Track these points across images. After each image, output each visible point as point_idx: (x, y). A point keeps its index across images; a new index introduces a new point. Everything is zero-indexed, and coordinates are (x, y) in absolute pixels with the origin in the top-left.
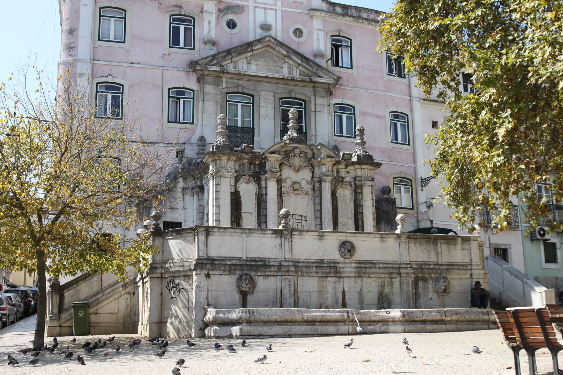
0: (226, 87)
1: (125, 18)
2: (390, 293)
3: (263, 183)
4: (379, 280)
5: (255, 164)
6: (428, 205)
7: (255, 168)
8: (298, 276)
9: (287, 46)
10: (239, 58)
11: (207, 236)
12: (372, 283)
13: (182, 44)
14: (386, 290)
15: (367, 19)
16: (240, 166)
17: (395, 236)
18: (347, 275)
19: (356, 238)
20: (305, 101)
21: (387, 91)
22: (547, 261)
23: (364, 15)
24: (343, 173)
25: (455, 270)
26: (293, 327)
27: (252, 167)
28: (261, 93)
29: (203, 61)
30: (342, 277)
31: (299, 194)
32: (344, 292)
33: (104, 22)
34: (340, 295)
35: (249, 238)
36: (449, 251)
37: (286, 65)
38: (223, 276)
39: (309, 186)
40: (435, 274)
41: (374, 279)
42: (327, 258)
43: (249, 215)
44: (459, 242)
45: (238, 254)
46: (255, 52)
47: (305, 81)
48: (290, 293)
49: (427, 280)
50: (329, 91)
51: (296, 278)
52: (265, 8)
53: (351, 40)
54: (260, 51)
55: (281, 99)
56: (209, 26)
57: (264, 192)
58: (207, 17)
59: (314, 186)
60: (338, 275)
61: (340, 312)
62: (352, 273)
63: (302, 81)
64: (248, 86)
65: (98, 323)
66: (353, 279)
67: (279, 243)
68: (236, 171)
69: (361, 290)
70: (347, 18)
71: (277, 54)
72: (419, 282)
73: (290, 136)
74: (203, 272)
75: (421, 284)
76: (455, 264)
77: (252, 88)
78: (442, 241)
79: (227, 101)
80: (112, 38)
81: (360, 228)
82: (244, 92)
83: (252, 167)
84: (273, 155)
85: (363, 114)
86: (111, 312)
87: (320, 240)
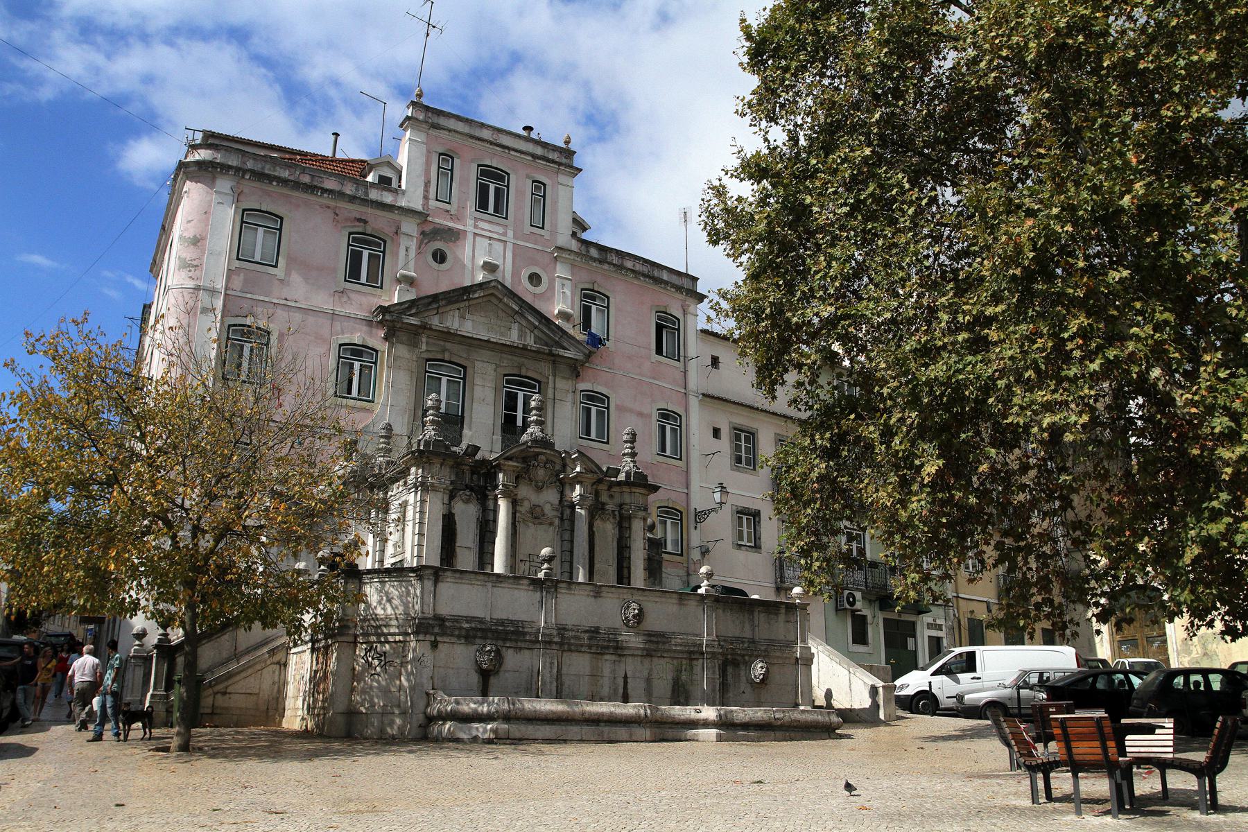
0: (427, 351)
1: (280, 230)
3: (491, 504)
4: (675, 662)
5: (478, 474)
6: (703, 550)
7: (479, 480)
8: (563, 651)
9: (520, 299)
10: (448, 308)
11: (436, 582)
13: (363, 279)
14: (684, 677)
15: (633, 271)
16: (457, 475)
17: (698, 598)
18: (631, 652)
20: (539, 382)
21: (654, 378)
22: (855, 642)
23: (629, 264)
24: (604, 498)
26: (570, 728)
27: (475, 477)
28: (477, 363)
30: (623, 655)
31: (541, 524)
32: (626, 678)
33: (247, 235)
34: (621, 682)
35: (495, 589)
37: (516, 326)
38: (455, 646)
39: (555, 513)
41: (667, 660)
42: (604, 624)
43: (467, 552)
45: (479, 613)
46: (471, 302)
47: (543, 353)
48: (551, 676)
50: (575, 370)
51: (560, 653)
52: (490, 238)
53: (608, 298)
54: (480, 300)
55: (505, 375)
56: (407, 255)
57: (491, 517)
58: (404, 242)
59: (562, 514)
60: (619, 652)
61: (635, 707)
62: (638, 649)
63: (538, 352)
64: (458, 352)
65: (226, 708)
66: (639, 659)
67: (539, 599)
68: (452, 483)
70: (606, 266)
71: (504, 308)
73: (532, 434)
74: (428, 638)
75: (730, 670)
77: (464, 355)
78: (761, 608)
79: (427, 372)
80: (257, 258)
81: (625, 581)
83: (475, 477)
84: (511, 463)
85: (620, 409)
86: (248, 691)
87: (595, 597)
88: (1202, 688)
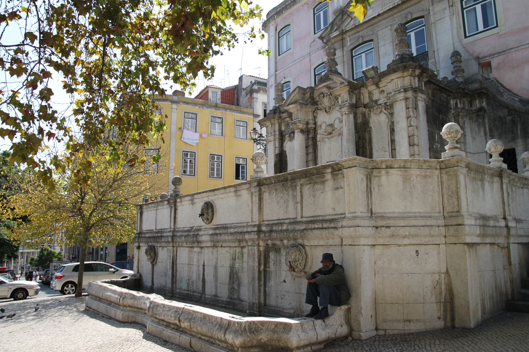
0: (351, 44)
2: (240, 268)
11: (480, 226)
12: (225, 255)
19: (216, 197)
25: (314, 231)
29: (325, 33)
31: (332, 137)
32: (204, 266)
34: (201, 268)
36: (314, 196)
40: (288, 239)
41: (227, 249)
44: (329, 176)
49: (280, 249)
69: (217, 263)
72: (271, 253)
75: (272, 256)
76: (321, 218)
78: (303, 181)
82: (365, 40)
88: (31, 121)
